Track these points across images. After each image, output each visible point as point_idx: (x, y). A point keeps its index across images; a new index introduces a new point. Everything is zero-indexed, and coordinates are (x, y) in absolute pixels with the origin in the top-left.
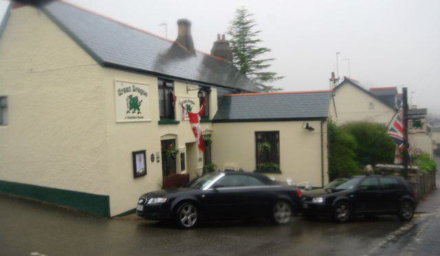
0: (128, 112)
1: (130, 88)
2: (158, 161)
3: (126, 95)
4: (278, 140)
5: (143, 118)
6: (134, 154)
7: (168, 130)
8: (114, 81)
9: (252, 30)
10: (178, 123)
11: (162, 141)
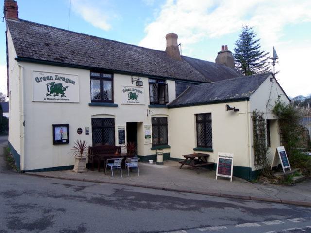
0: (129, 100)
3: (44, 83)
4: (210, 121)
5: (68, 100)
7: (103, 112)
9: (254, 39)
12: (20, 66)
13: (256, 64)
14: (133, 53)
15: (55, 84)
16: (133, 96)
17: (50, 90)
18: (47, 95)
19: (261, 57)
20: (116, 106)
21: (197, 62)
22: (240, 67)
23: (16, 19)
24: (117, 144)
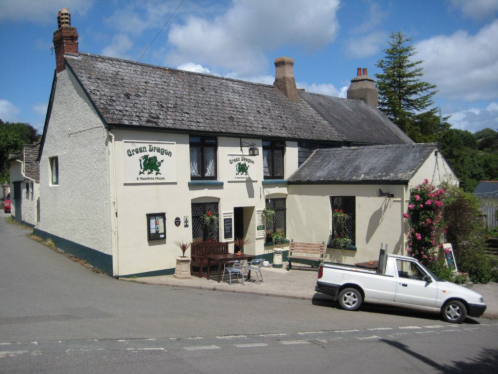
1: (145, 148)
2: (186, 226)
6: (150, 216)
9: (411, 59)
13: (412, 101)
14: (231, 96)
15: (149, 157)
16: (242, 169)
18: (141, 173)
21: (321, 100)
22: (386, 104)
23: (75, 54)
24: (222, 240)
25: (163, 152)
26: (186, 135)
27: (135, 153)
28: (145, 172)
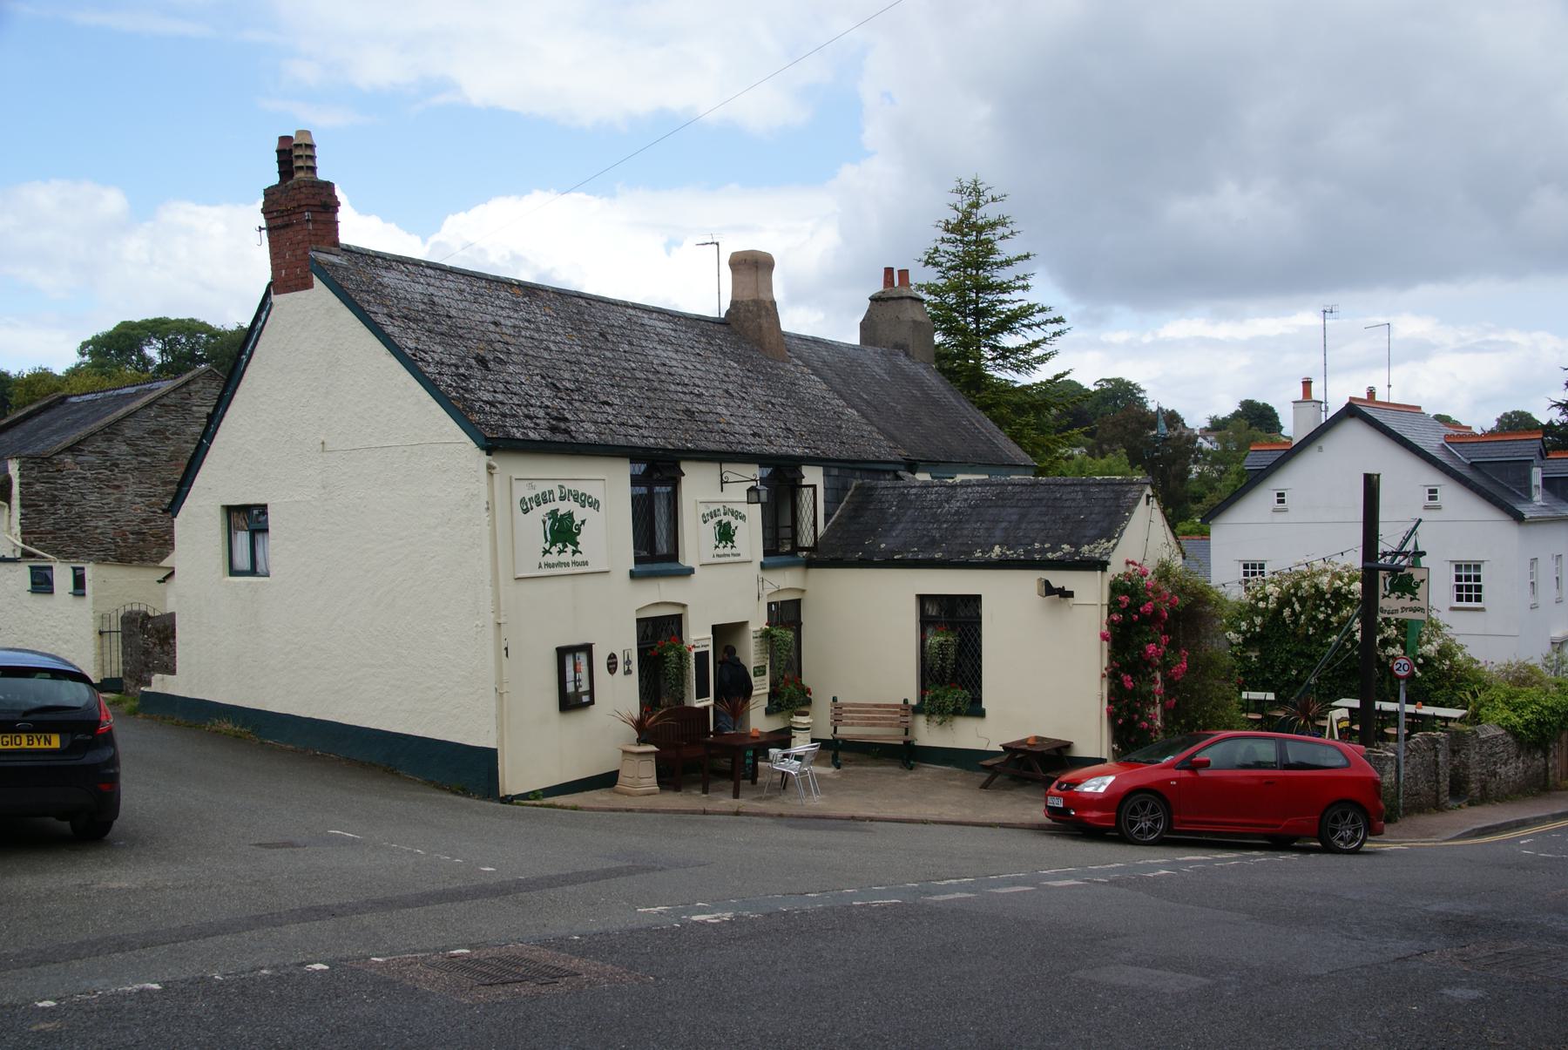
0: (546, 552)
1: (551, 492)
2: (628, 672)
5: (586, 563)
6: (562, 653)
7: (660, 594)
8: (511, 478)
10: (689, 572)
11: (639, 621)
12: (490, 467)
15: (723, 522)
17: (1388, 588)
19: (1029, 326)
20: (689, 572)
25: (584, 501)
26: (625, 459)
27: (534, 505)
28: (1392, 595)
